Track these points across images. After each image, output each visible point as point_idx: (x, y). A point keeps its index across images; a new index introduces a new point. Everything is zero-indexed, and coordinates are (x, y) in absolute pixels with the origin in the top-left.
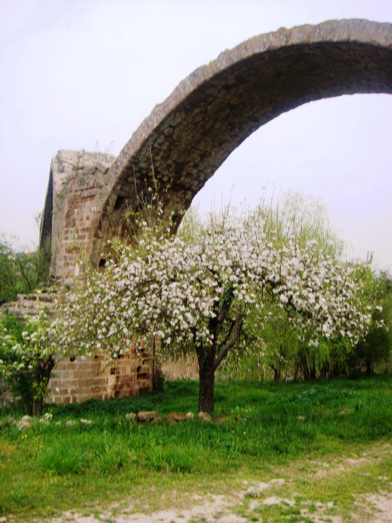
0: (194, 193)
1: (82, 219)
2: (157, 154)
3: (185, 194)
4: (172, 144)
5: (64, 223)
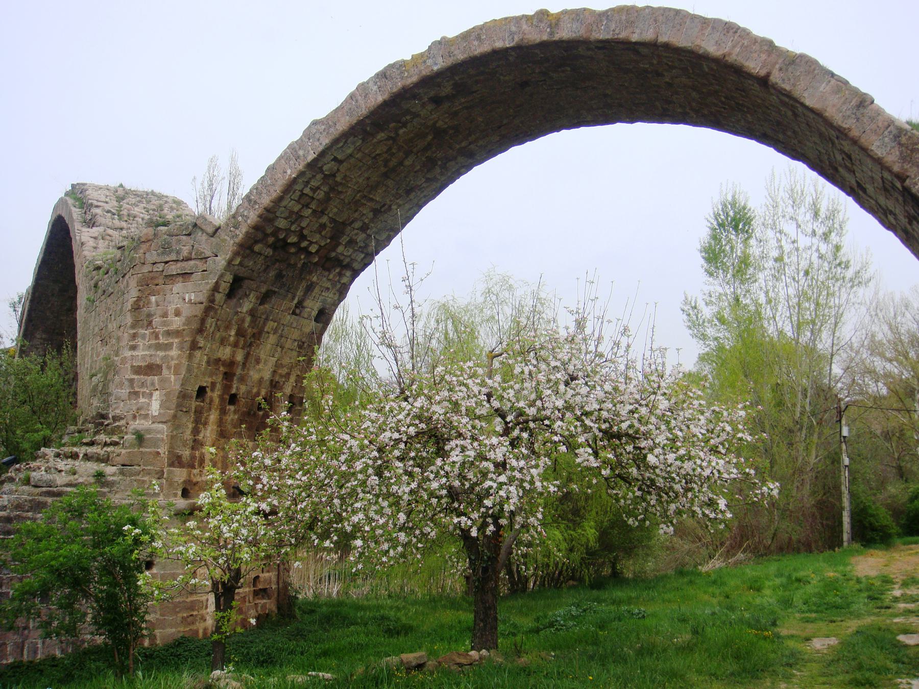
0: (356, 274)
1: (165, 315)
2: (307, 206)
3: (340, 275)
4: (332, 189)
5: (129, 320)
